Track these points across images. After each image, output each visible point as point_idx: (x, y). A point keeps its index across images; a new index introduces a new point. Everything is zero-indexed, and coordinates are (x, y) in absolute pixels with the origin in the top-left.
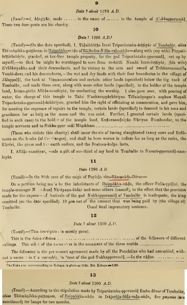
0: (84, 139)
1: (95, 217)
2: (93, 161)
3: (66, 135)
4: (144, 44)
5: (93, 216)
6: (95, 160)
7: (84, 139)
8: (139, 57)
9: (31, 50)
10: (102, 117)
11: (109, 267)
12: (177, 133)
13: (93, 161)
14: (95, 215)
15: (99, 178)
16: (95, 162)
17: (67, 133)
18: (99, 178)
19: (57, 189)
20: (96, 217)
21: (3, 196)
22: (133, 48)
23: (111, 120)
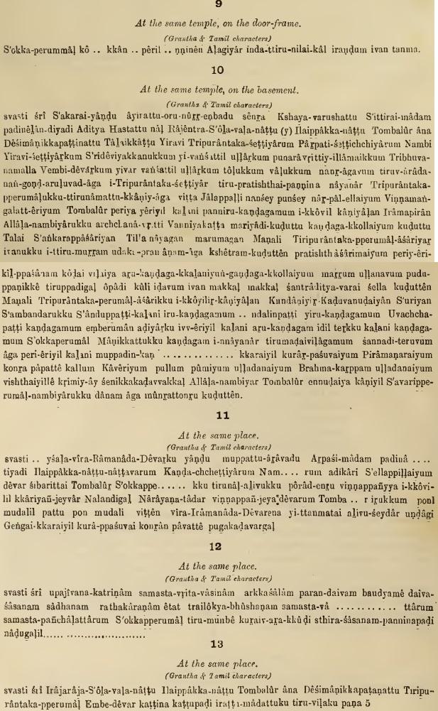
0: (75, 369)
1: (217, 549)
2: (223, 416)
3: (270, 203)
4: (321, 155)
5: (214, 547)
6: (306, 474)
7: (75, 369)
8: (60, 486)
9: (193, 525)
10: (272, 293)
11: (246, 708)
12: (302, 369)
13: (223, 416)
14: (219, 546)
15: (98, 277)
16: (227, 418)
17: (289, 132)
18: (98, 277)
19: (147, 497)
20: (220, 549)
21: (7, 514)
22: (218, 281)
23: (387, 274)
